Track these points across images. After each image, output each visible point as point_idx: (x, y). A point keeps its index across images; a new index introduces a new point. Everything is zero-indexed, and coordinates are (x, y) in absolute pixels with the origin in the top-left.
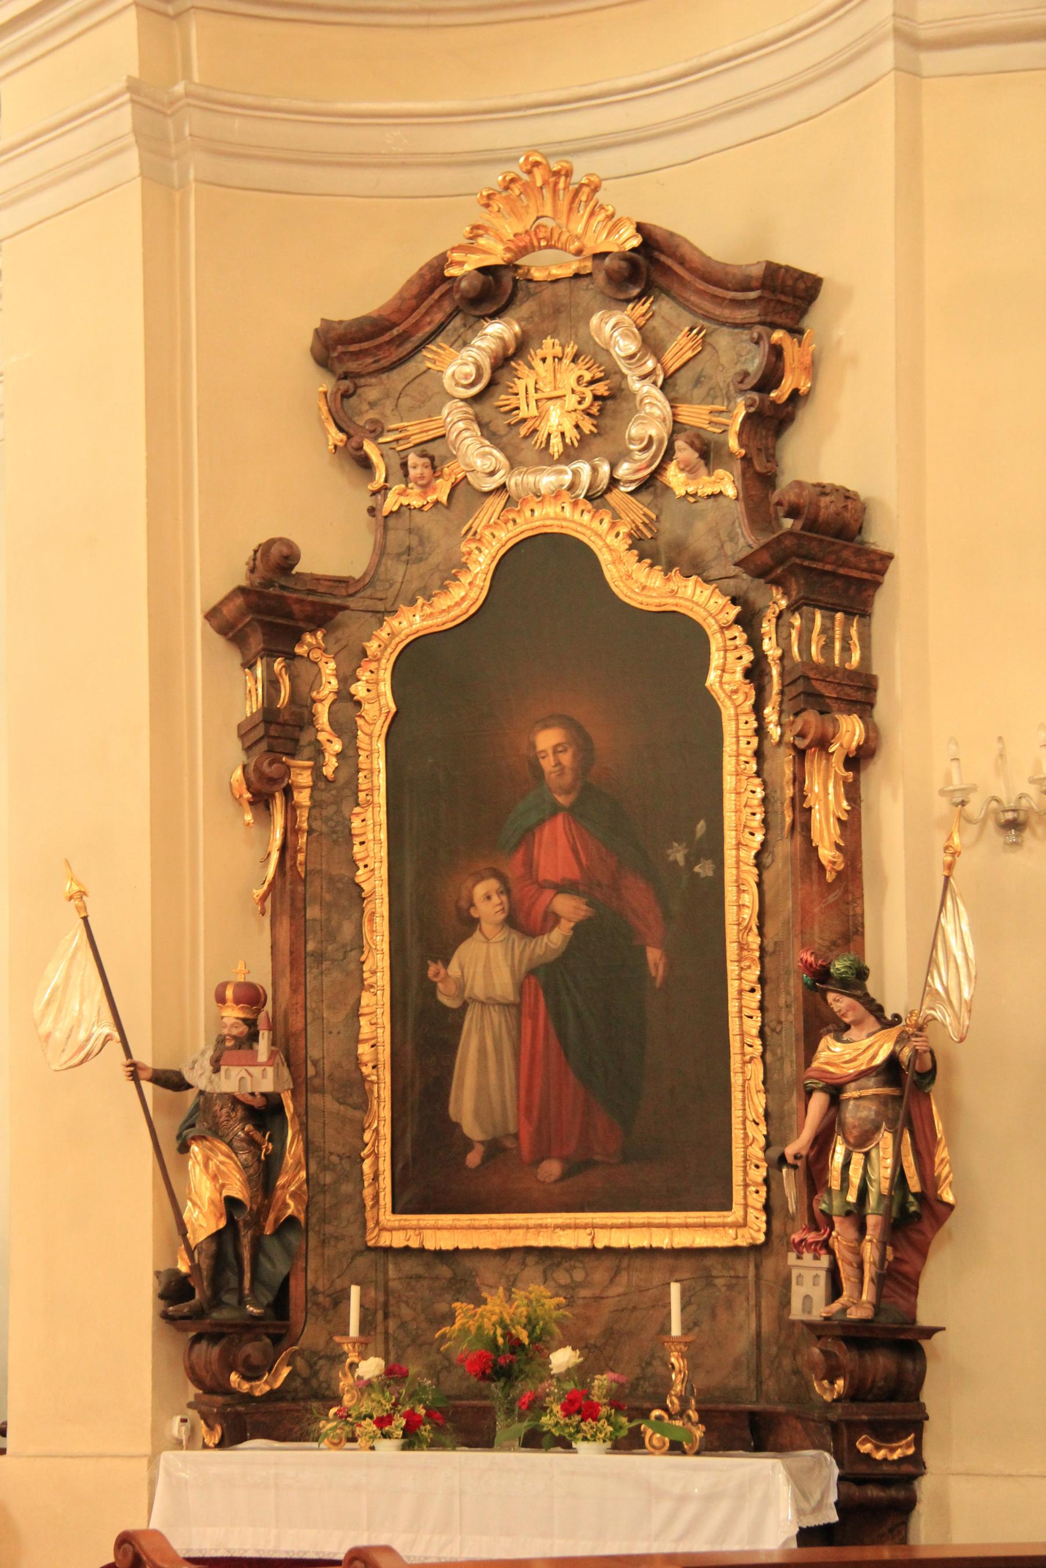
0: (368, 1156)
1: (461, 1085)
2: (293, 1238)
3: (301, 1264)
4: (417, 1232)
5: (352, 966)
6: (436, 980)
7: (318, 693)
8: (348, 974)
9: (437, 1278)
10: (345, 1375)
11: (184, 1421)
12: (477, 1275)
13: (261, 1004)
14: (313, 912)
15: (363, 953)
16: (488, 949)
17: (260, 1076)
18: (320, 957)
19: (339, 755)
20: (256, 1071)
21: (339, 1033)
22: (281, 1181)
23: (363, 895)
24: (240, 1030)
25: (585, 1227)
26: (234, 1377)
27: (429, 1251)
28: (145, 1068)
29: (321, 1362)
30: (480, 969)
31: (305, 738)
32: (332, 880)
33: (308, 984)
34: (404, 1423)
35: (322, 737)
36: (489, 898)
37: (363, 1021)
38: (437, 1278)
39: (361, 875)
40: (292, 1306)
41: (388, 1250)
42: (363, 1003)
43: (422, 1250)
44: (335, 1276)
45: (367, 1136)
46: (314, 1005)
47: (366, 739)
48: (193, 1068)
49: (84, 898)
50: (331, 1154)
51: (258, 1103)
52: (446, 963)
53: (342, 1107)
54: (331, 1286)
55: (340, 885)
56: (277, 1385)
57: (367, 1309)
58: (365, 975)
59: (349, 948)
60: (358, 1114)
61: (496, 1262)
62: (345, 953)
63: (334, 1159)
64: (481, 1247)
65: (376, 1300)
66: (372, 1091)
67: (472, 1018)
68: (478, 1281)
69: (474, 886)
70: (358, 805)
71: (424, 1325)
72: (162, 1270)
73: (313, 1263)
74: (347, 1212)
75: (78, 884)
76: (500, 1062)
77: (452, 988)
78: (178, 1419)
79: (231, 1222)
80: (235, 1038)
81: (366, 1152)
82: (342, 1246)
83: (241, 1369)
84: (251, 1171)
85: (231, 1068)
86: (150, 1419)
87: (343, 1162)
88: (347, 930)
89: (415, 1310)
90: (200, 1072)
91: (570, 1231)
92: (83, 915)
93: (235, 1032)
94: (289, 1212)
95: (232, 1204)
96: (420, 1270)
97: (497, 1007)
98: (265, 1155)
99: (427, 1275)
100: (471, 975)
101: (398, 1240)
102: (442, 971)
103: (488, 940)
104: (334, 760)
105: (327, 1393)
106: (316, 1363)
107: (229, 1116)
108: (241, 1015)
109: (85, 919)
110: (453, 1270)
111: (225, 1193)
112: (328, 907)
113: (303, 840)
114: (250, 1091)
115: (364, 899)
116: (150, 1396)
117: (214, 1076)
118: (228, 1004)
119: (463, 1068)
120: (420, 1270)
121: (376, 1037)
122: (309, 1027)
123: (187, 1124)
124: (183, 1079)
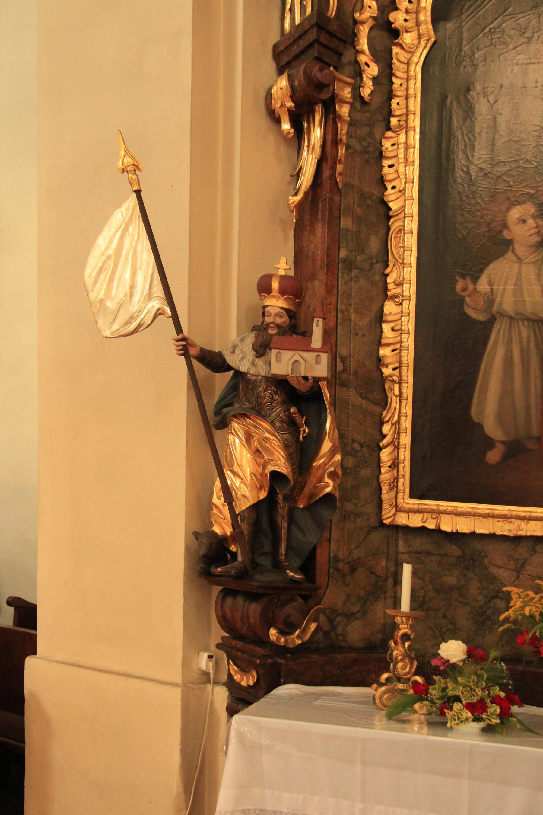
0: (386, 446)
1: (485, 391)
2: (324, 512)
3: (326, 535)
4: (434, 516)
5: (377, 278)
6: (463, 294)
7: (361, 14)
8: (373, 283)
9: (446, 555)
10: (396, 643)
11: (210, 657)
12: (486, 556)
13: (302, 299)
14: (346, 223)
15: (387, 266)
16: (520, 268)
17: (314, 362)
18: (349, 264)
19: (374, 79)
20: (310, 356)
21: (364, 335)
22: (318, 463)
23: (391, 213)
24: (284, 319)
25: (431, 512)
26: (273, 632)
27: (445, 533)
28: (193, 345)
29: (339, 618)
30: (510, 287)
31: (347, 57)
32: (362, 196)
33: (340, 287)
34: (498, 711)
35: (362, 59)
36: (524, 221)
37: (386, 328)
38: (446, 555)
39: (390, 194)
40: (318, 572)
41: (406, 528)
42: (386, 311)
43: (438, 531)
44: (353, 547)
45: (386, 429)
46: (344, 308)
47: (403, 67)
48: (233, 352)
49: (138, 172)
50: (354, 441)
51: (303, 387)
52: (475, 279)
53: (364, 402)
54: (350, 554)
55: (369, 202)
56: (307, 637)
57: (378, 576)
58: (390, 286)
59: (375, 261)
60: (377, 409)
61: (506, 546)
62: (372, 264)
63: (356, 446)
64: (499, 533)
65: (387, 569)
66: (392, 390)
67: (499, 330)
68: (486, 561)
69: (509, 209)
70: (389, 129)
71: (431, 594)
72: (201, 531)
73: (335, 534)
74: (365, 492)
75: (133, 158)
76: (526, 371)
77: (481, 303)
78: (206, 655)
79: (272, 493)
80: (278, 326)
81: (385, 441)
82: (359, 521)
83: (280, 626)
84: (291, 450)
85: (282, 351)
86: (181, 654)
87: (364, 449)
88: (374, 244)
89: (423, 580)
90: (240, 356)
91: (490, 519)
92: (136, 188)
93: (279, 321)
94: (328, 490)
95: (276, 476)
96: (430, 547)
97: (526, 323)
98: (303, 438)
99: (435, 552)
100: (500, 292)
101: (415, 521)
102: (471, 287)
103: (520, 260)
104: (370, 83)
105: (343, 644)
106: (335, 619)
107: (272, 398)
108: (285, 306)
109: (138, 192)
110: (463, 550)
111: (271, 468)
112: (358, 220)
113: (342, 151)
114: (303, 375)
115: (391, 217)
116: (181, 636)
117: (257, 360)
118: (274, 294)
119: (488, 373)
120: (430, 547)
121: (401, 342)
122: (339, 327)
123: (223, 402)
124: (224, 360)
